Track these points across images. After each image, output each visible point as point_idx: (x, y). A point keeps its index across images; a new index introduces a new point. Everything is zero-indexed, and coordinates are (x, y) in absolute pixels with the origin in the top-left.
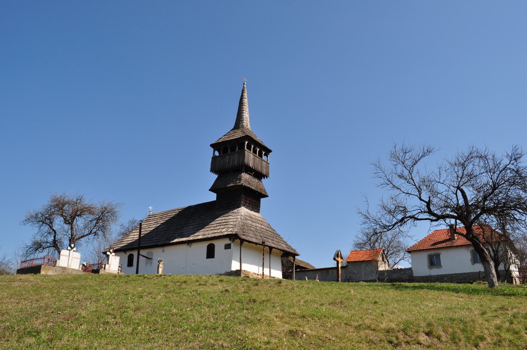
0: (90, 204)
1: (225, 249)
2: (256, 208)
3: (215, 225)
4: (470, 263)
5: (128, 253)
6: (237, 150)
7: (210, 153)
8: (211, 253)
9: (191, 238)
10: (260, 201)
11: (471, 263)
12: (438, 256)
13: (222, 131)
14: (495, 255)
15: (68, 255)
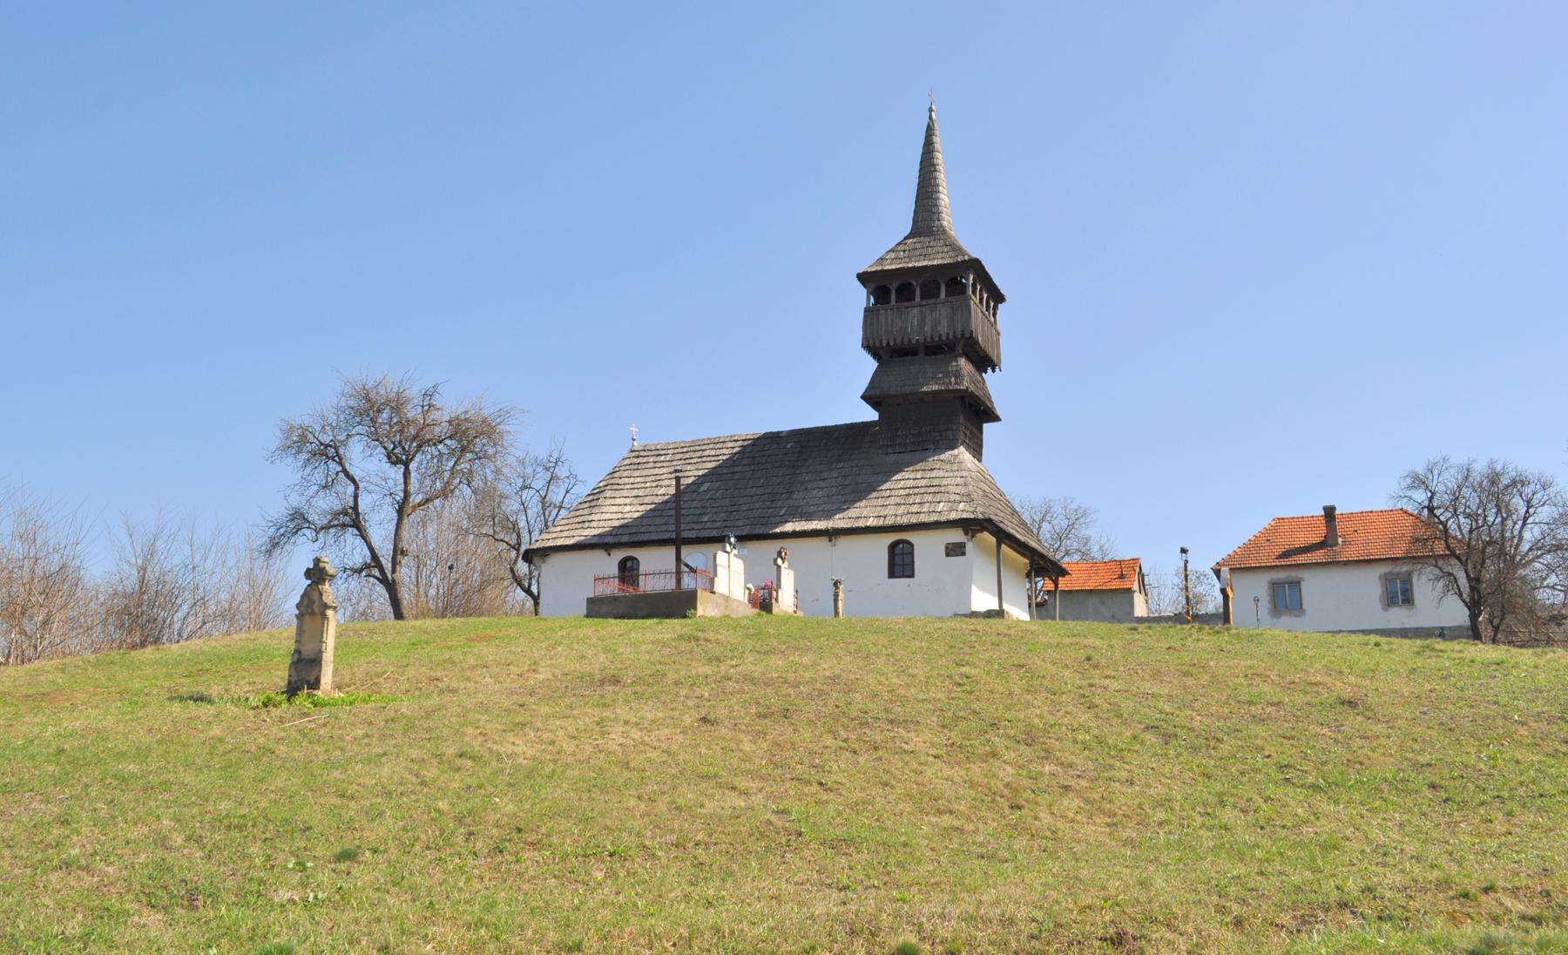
0: (461, 410)
1: (948, 555)
2: (977, 451)
3: (902, 492)
4: (1377, 605)
5: (619, 555)
6: (943, 295)
7: (860, 297)
8: (901, 563)
9: (839, 522)
10: (981, 431)
11: (1379, 606)
12: (1296, 584)
13: (882, 235)
14: (1472, 589)
15: (672, 566)
